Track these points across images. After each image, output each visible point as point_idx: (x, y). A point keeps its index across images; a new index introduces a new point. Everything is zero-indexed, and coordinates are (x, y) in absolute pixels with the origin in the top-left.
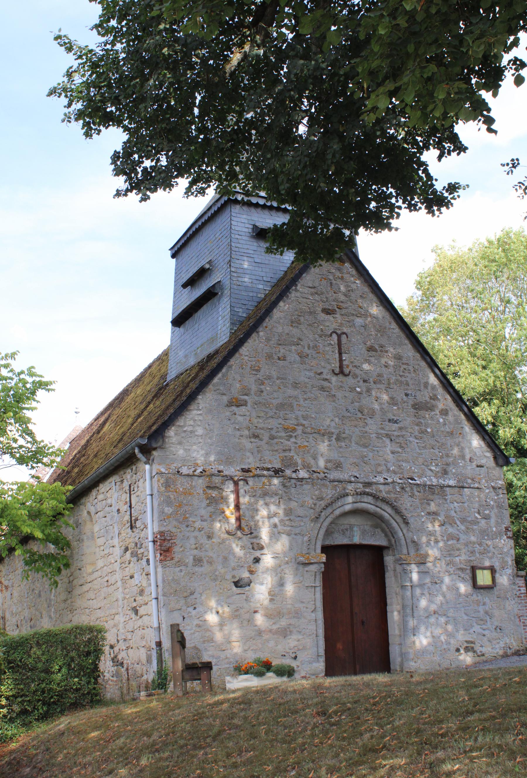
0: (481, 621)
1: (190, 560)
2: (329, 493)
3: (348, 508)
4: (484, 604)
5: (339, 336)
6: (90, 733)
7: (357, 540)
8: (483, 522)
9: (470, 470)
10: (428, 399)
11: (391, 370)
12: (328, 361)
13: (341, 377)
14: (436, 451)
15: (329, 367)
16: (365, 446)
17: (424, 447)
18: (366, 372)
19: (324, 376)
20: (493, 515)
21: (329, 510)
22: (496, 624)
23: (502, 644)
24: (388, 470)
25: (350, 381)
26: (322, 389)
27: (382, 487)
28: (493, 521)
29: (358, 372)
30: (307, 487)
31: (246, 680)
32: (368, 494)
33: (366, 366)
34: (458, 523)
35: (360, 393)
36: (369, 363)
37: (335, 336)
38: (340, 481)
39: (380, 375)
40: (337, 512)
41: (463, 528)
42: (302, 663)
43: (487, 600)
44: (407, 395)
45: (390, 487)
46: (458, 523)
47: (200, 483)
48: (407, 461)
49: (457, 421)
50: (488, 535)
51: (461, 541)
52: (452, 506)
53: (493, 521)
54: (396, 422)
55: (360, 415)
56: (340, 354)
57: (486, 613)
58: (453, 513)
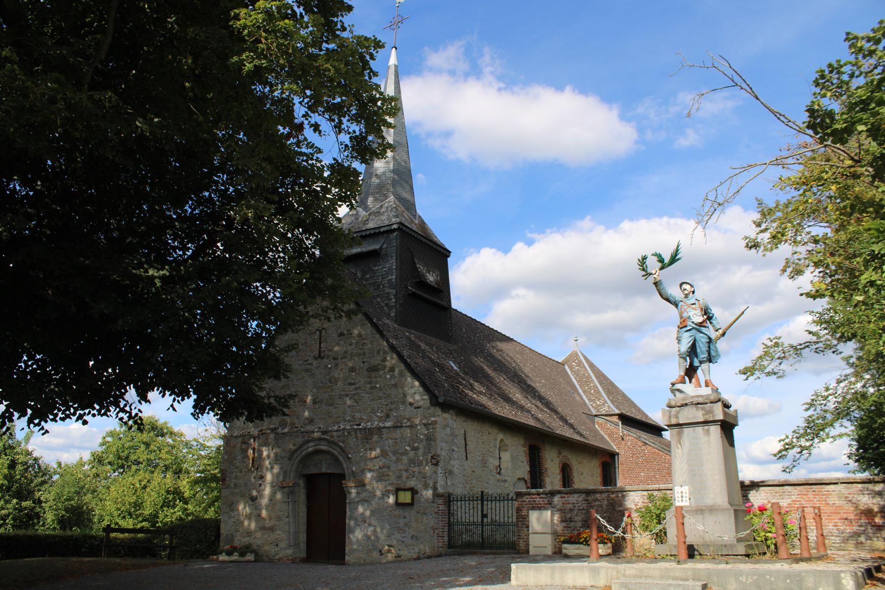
0: (400, 530)
1: (232, 485)
2: (300, 440)
3: (310, 449)
4: (405, 517)
5: (321, 332)
6: (441, 577)
7: (324, 470)
8: (412, 453)
9: (408, 412)
10: (380, 362)
11: (354, 346)
12: (312, 351)
13: (319, 360)
14: (383, 401)
15: (313, 355)
16: (330, 405)
17: (373, 400)
18: (336, 353)
19: (310, 362)
20: (421, 446)
21: (299, 452)
22: (413, 533)
23: (417, 550)
24: (345, 420)
25: (325, 361)
26: (307, 371)
27: (334, 434)
28: (421, 451)
29: (330, 353)
30: (287, 438)
31: (578, 549)
32: (324, 439)
33: (336, 349)
34: (391, 455)
35: (330, 368)
36: (338, 344)
37: (318, 333)
38: (307, 432)
39: (346, 352)
40: (303, 453)
41: (394, 458)
42: (281, 549)
43: (407, 514)
44: (363, 362)
45: (340, 433)
46: (391, 455)
47: (240, 440)
48: (360, 412)
49: (401, 374)
50: (414, 464)
51: (392, 469)
52: (387, 442)
53: (421, 451)
54: (353, 384)
55: (329, 384)
56: (320, 344)
57: (406, 524)
58: (387, 448)
